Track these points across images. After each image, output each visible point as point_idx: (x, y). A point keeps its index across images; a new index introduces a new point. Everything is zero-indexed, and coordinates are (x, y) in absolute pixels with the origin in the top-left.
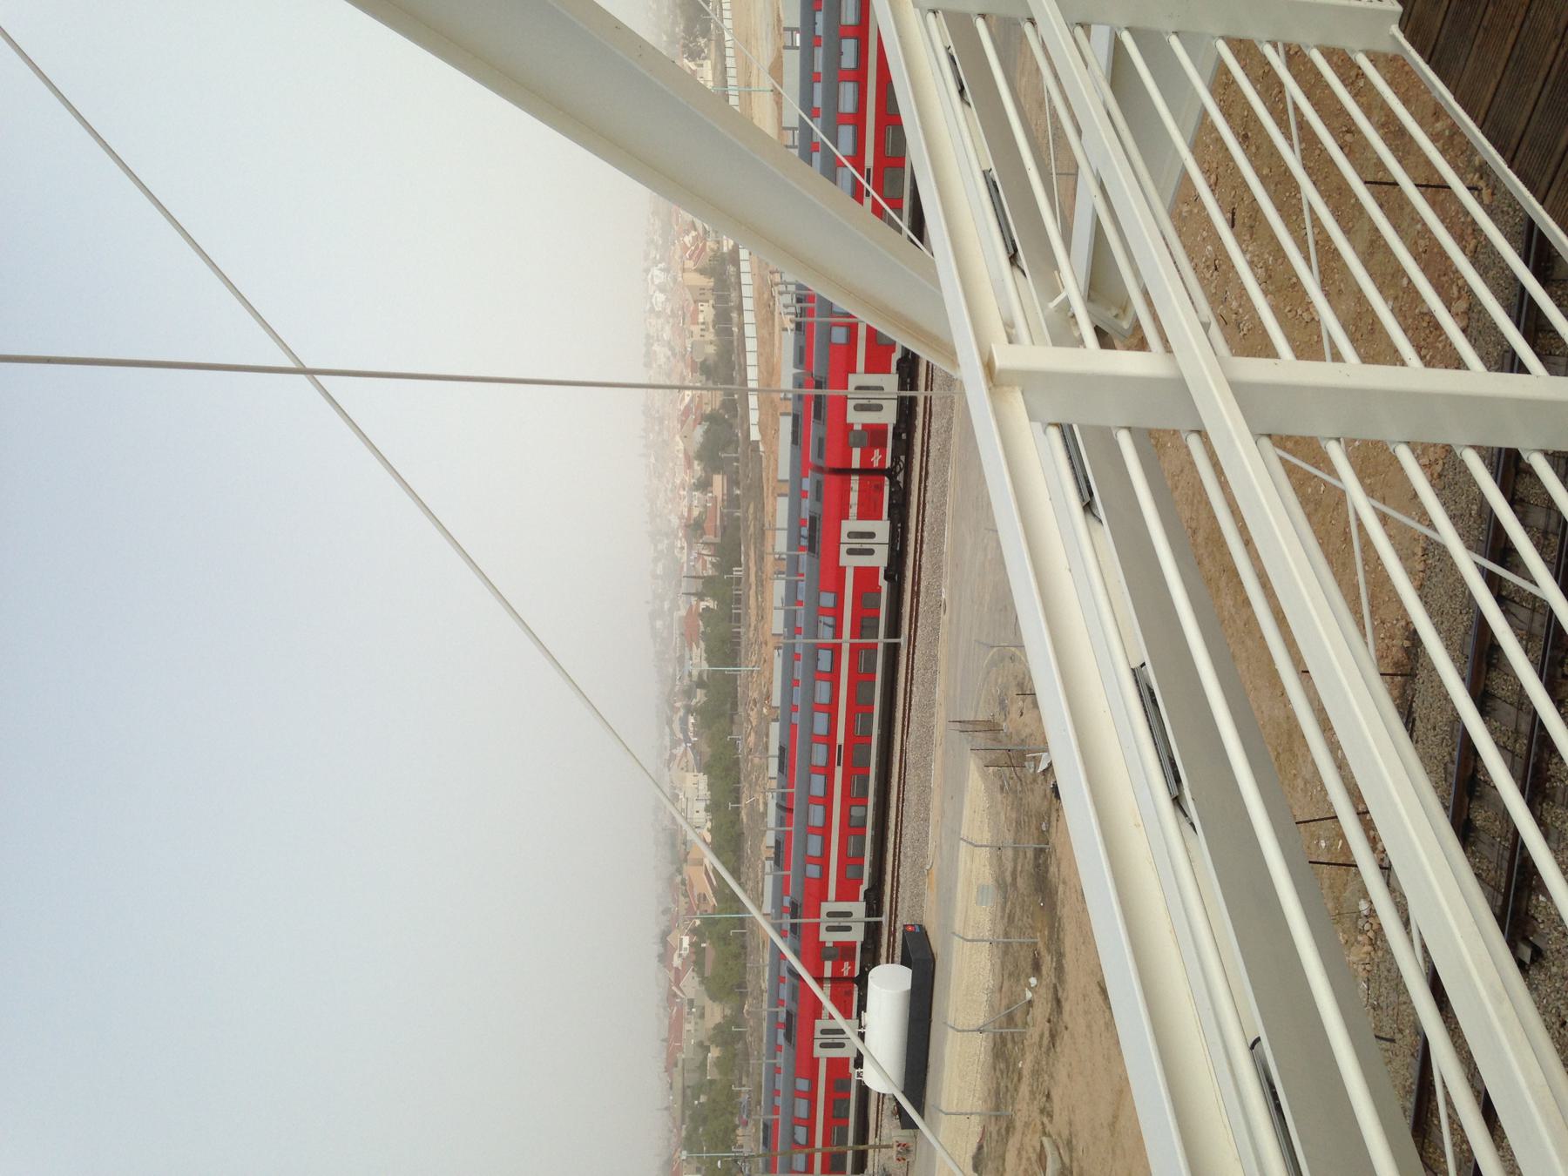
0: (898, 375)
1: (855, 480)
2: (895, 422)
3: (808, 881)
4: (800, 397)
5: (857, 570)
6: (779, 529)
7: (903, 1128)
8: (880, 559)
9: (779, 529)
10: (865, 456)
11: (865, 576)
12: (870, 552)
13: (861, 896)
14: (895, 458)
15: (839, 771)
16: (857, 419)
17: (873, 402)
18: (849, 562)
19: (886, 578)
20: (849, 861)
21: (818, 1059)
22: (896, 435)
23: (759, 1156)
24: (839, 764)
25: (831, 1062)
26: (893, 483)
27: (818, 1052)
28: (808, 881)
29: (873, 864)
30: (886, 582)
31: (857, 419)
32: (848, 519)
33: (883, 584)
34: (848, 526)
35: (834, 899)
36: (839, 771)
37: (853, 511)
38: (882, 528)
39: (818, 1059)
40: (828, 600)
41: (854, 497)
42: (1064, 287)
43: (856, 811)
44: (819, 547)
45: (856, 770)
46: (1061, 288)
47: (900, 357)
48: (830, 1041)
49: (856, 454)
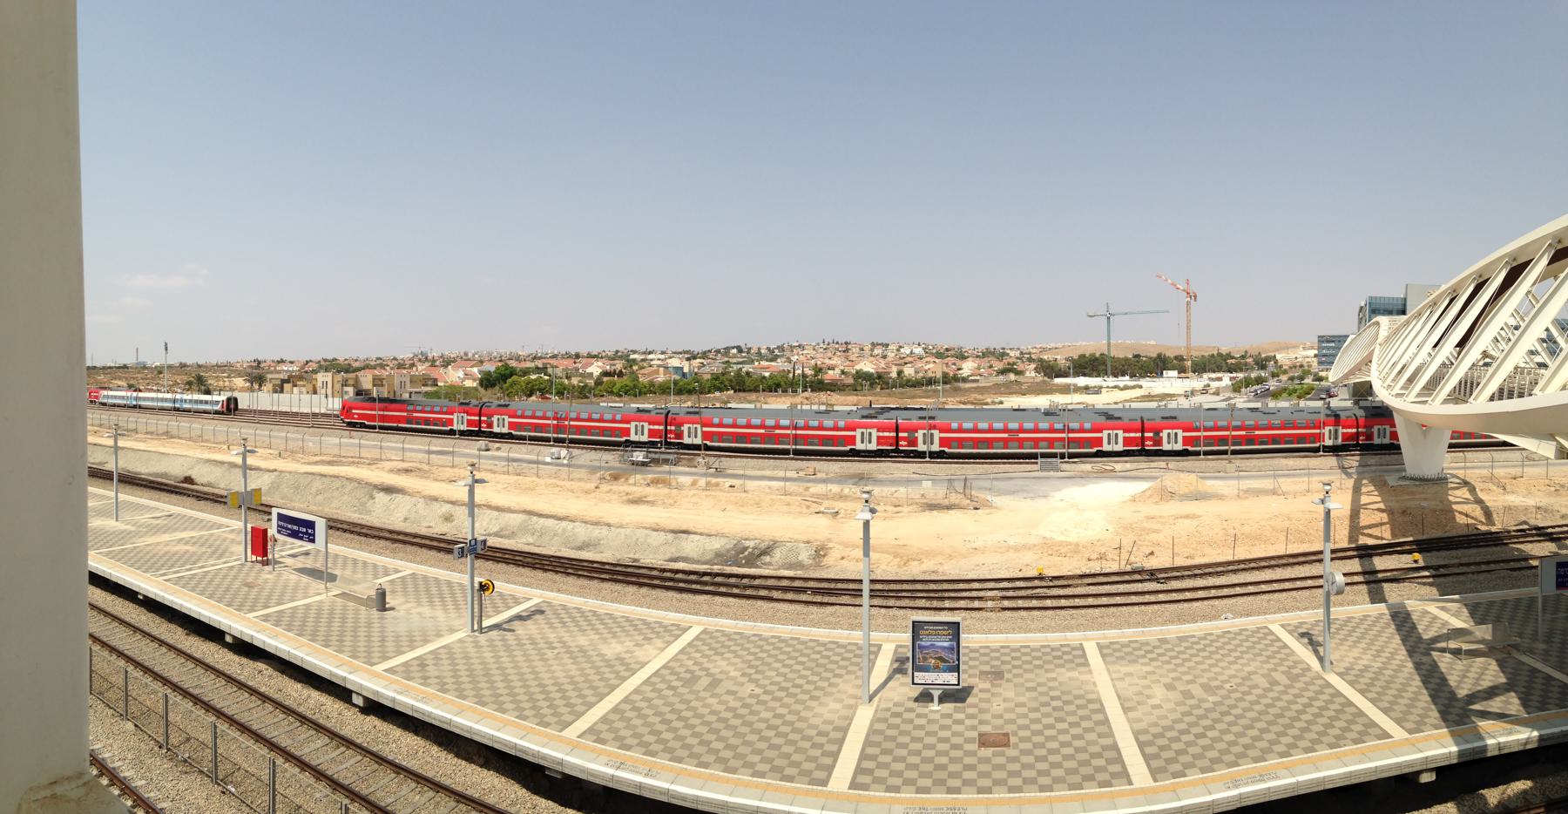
3: (516, 411)
5: (855, 436)
7: (1372, 603)
10: (904, 439)
11: (627, 432)
12: (1109, 443)
14: (903, 451)
15: (762, 431)
16: (920, 434)
18: (632, 426)
20: (721, 436)
22: (912, 451)
26: (892, 451)
28: (516, 411)
29: (959, 453)
31: (495, 419)
36: (762, 431)
37: (652, 427)
38: (873, 446)
40: (618, 417)
41: (656, 427)
42: (1175, 418)
43: (1042, 444)
44: (639, 414)
45: (763, 439)
46: (1174, 421)
49: (905, 435)
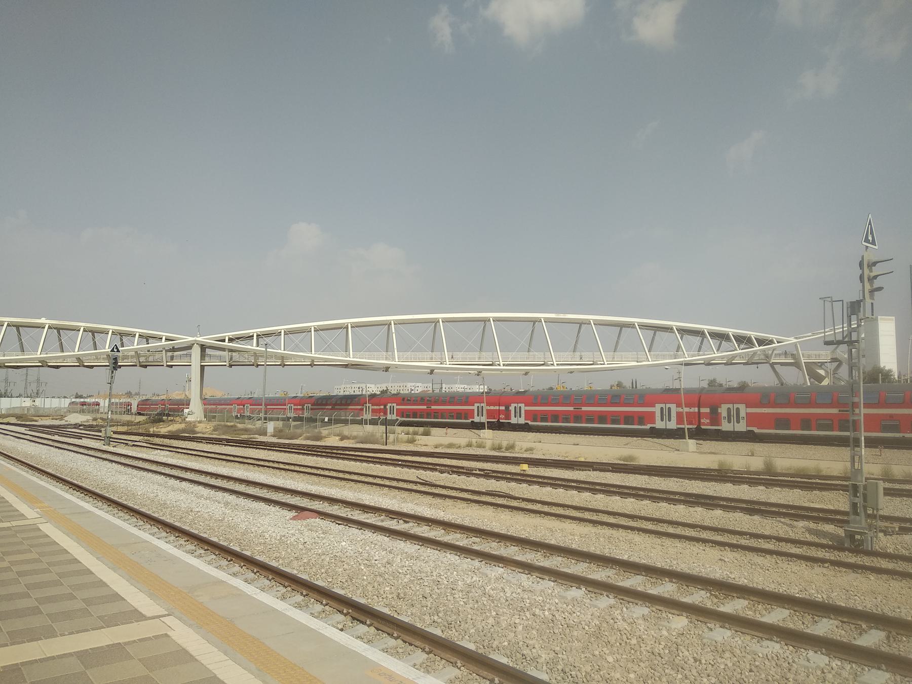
0: (676, 428)
1: (696, 410)
2: (723, 430)
4: (285, 400)
5: (654, 413)
6: (655, 334)
8: (659, 425)
9: (655, 334)
11: (651, 417)
13: (750, 428)
17: (665, 417)
18: (657, 409)
19: (472, 421)
21: (655, 407)
23: (544, 354)
24: (574, 409)
25: (653, 414)
27: (658, 407)
30: (649, 428)
32: (677, 407)
33: (648, 426)
34: (742, 407)
35: (747, 412)
38: (742, 427)
39: (655, 407)
47: (755, 432)
48: (664, 413)
